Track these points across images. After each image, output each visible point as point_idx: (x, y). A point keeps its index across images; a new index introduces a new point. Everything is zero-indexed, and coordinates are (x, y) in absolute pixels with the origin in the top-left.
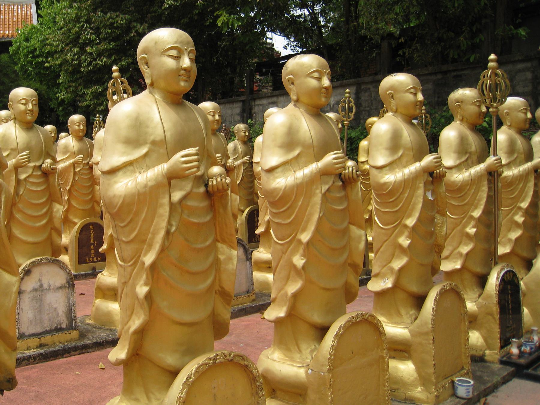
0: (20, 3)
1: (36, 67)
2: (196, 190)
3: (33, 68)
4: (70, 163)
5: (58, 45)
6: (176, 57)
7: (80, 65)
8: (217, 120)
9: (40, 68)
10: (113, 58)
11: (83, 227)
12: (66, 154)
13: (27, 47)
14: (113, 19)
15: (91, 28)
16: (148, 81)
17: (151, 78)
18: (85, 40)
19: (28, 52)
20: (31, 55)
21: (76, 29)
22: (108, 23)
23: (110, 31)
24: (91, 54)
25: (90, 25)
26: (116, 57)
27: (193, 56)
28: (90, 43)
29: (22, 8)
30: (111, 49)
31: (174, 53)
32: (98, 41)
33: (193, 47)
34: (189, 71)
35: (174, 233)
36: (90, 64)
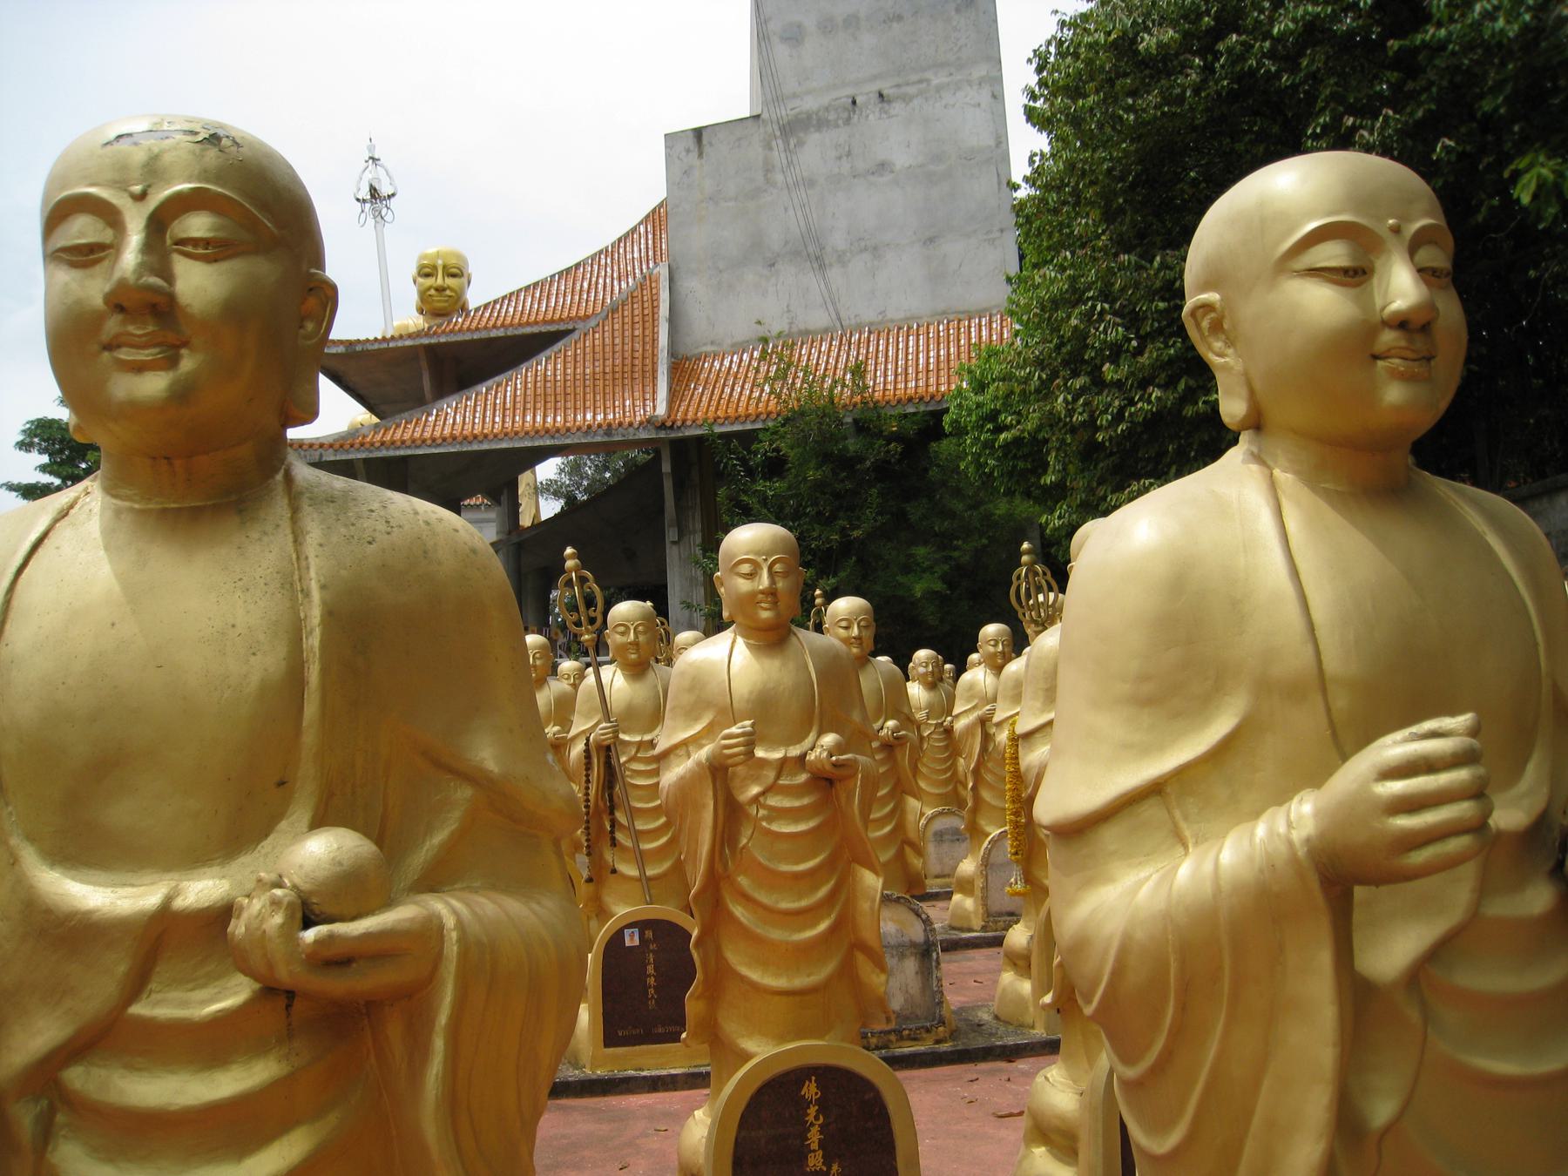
0: (985, 310)
1: (1005, 455)
2: (1502, 907)
3: (998, 459)
4: (699, 764)
5: (1029, 377)
6: (1345, 271)
7: (1091, 425)
8: (1402, 323)
9: (1015, 457)
10: (1182, 386)
11: (760, 1091)
12: (697, 719)
13: (979, 405)
14: (1171, 268)
15: (1115, 314)
16: (1232, 408)
17: (1244, 392)
18: (1102, 350)
19: (981, 418)
20: (989, 426)
21: (1074, 322)
22: (1158, 284)
23: (1162, 305)
24: (1119, 384)
25: (1112, 303)
26: (1192, 383)
27: (1437, 257)
28: (1116, 352)
29: (991, 322)
30: (1171, 361)
31: (1333, 254)
32: (1134, 343)
33: (1428, 214)
34: (1426, 328)
35: (1389, 1128)
36: (1119, 417)
